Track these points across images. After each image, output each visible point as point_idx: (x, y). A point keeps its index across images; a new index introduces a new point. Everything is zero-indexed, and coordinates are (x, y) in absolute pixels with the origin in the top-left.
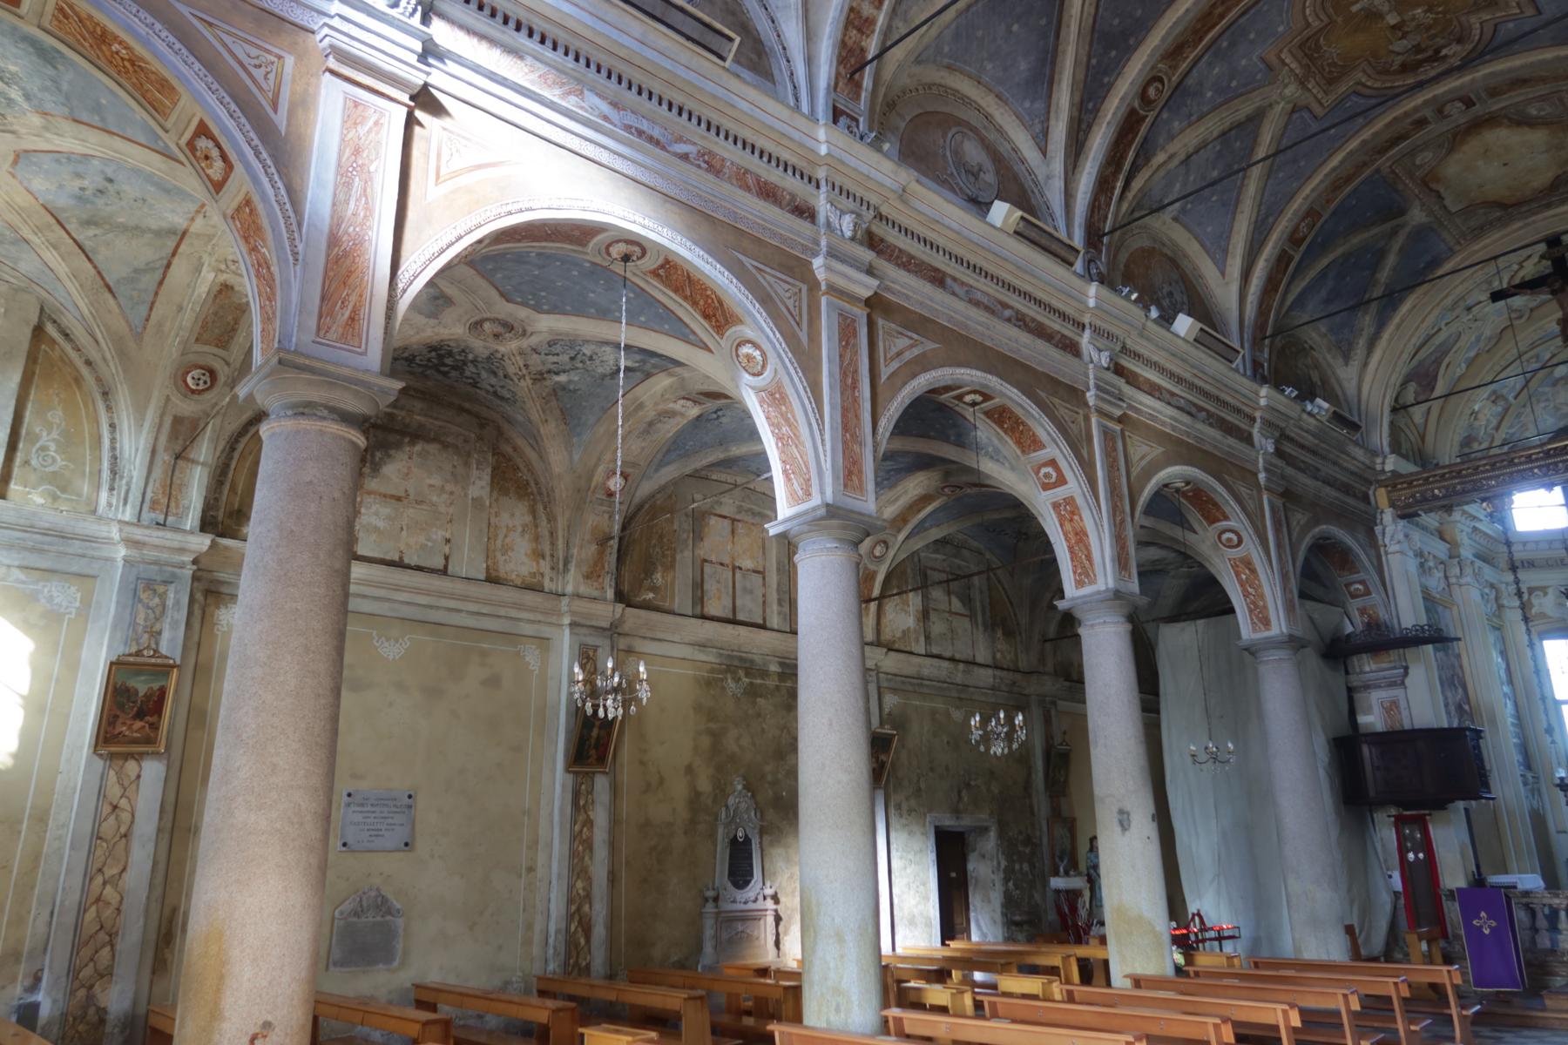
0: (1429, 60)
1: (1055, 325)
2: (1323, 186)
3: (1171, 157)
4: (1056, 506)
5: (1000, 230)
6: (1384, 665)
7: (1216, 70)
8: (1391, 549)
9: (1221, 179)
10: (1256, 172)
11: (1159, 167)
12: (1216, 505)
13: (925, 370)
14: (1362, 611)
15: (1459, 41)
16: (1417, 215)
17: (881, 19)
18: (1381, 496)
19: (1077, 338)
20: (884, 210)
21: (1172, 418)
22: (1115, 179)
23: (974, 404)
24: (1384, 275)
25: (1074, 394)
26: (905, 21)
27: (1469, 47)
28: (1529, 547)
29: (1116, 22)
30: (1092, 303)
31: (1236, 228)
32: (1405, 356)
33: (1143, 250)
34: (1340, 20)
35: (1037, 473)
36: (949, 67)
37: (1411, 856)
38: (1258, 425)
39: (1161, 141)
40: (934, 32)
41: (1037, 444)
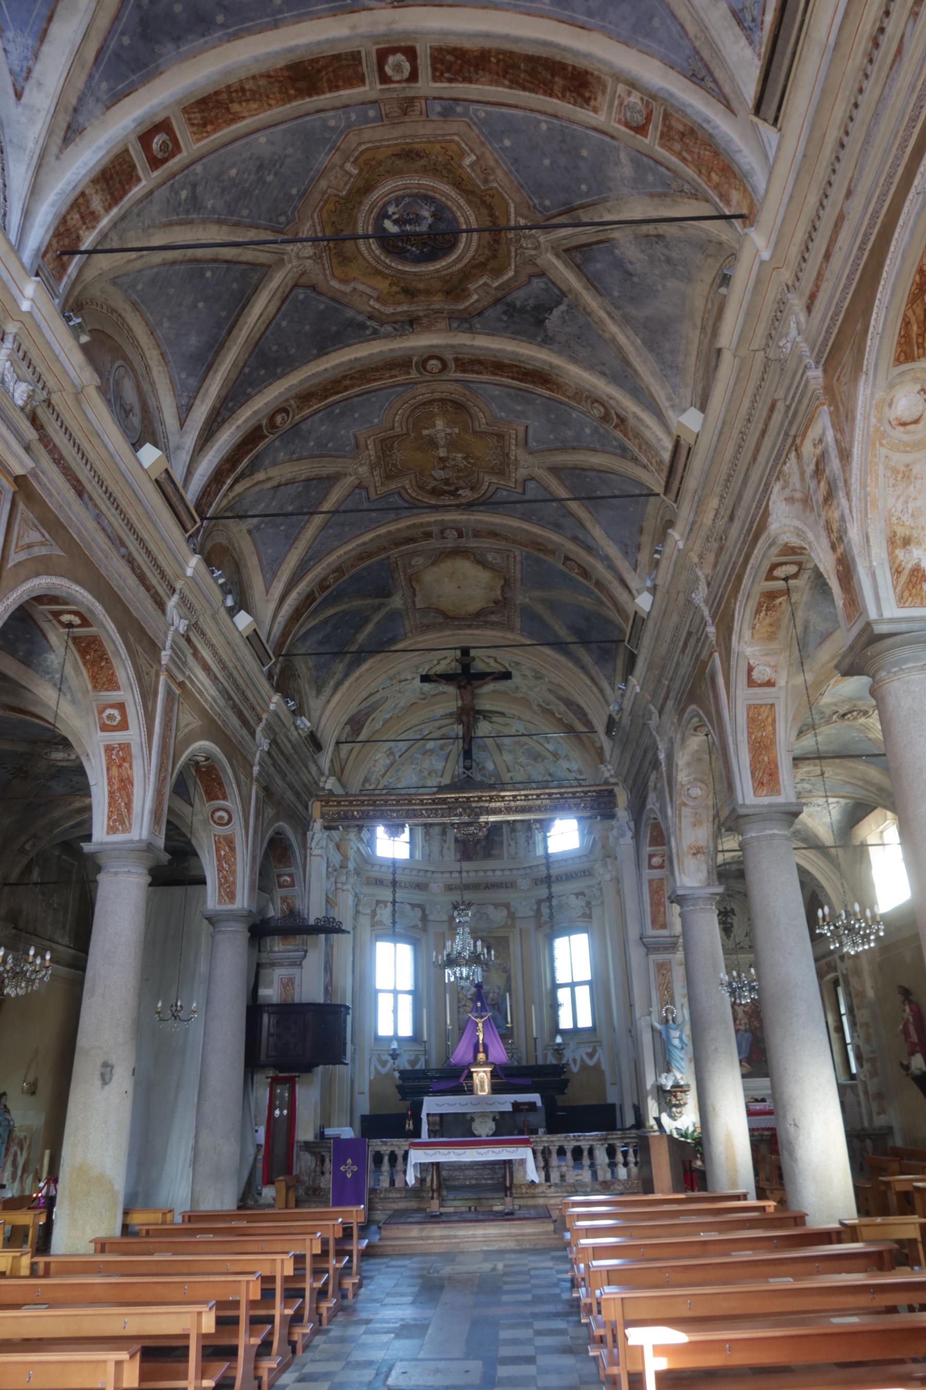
0: (449, 492)
1: (154, 580)
2: (353, 553)
3: (269, 479)
4: (109, 749)
5: (145, 471)
6: (290, 947)
7: (323, 428)
8: (315, 852)
9: (292, 514)
10: (318, 520)
11: (258, 483)
12: (221, 784)
13: (48, 574)
14: (284, 900)
15: (472, 489)
16: (397, 602)
17: (105, 222)
18: (316, 808)
19: (165, 598)
20: (55, 399)
21: (213, 698)
22: (228, 477)
23: (70, 625)
24: (361, 637)
25: (154, 649)
26: (121, 239)
27: (476, 496)
28: (383, 869)
29: (275, 348)
30: (189, 572)
31: (288, 559)
32: (355, 703)
33: (221, 545)
34: (413, 435)
35: (101, 712)
36: (134, 304)
37: (277, 1112)
38: (262, 725)
39: (267, 462)
40: (138, 265)
41: (112, 684)
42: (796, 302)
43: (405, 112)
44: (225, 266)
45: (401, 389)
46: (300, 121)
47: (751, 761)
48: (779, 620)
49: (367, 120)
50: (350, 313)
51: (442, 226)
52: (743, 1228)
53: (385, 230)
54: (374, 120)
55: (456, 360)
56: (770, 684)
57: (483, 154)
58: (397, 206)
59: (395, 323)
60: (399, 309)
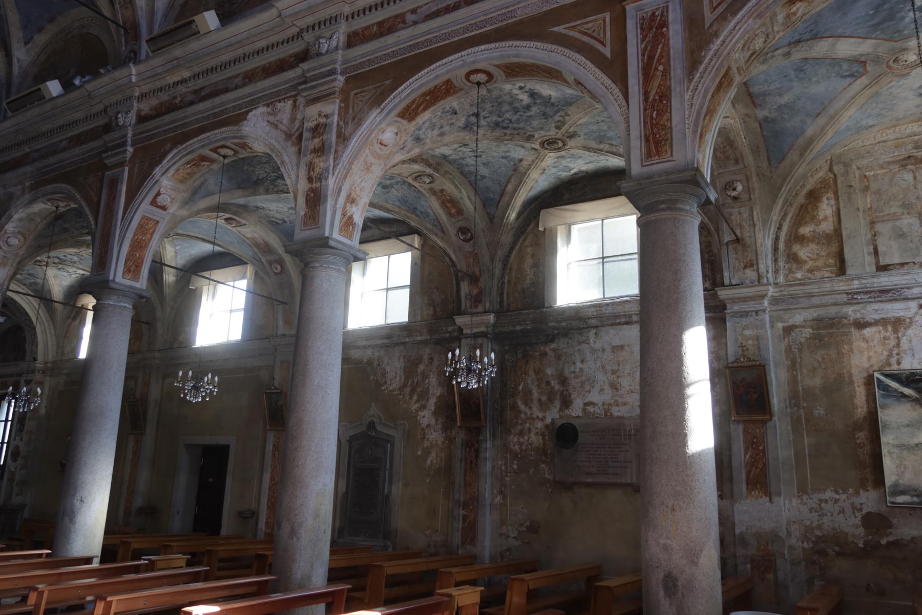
42: (343, 27)
47: (128, 253)
48: (195, 173)
52: (36, 569)
56: (164, 208)
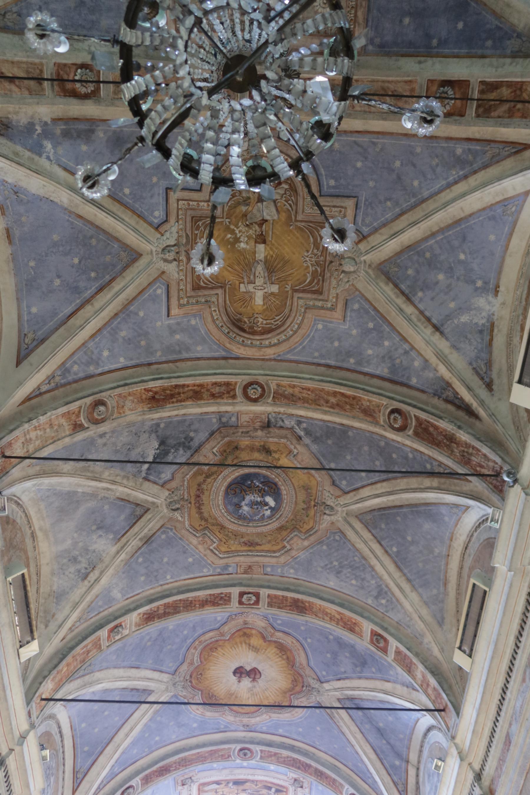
7: (370, 352)
36: (445, 584)
43: (250, 567)
44: (383, 543)
45: (290, 357)
46: (309, 580)
49: (272, 567)
50: (314, 447)
51: (235, 500)
53: (275, 500)
54: (268, 566)
55: (234, 397)
57: (205, 551)
58: (264, 515)
59: (281, 427)
60: (276, 440)
